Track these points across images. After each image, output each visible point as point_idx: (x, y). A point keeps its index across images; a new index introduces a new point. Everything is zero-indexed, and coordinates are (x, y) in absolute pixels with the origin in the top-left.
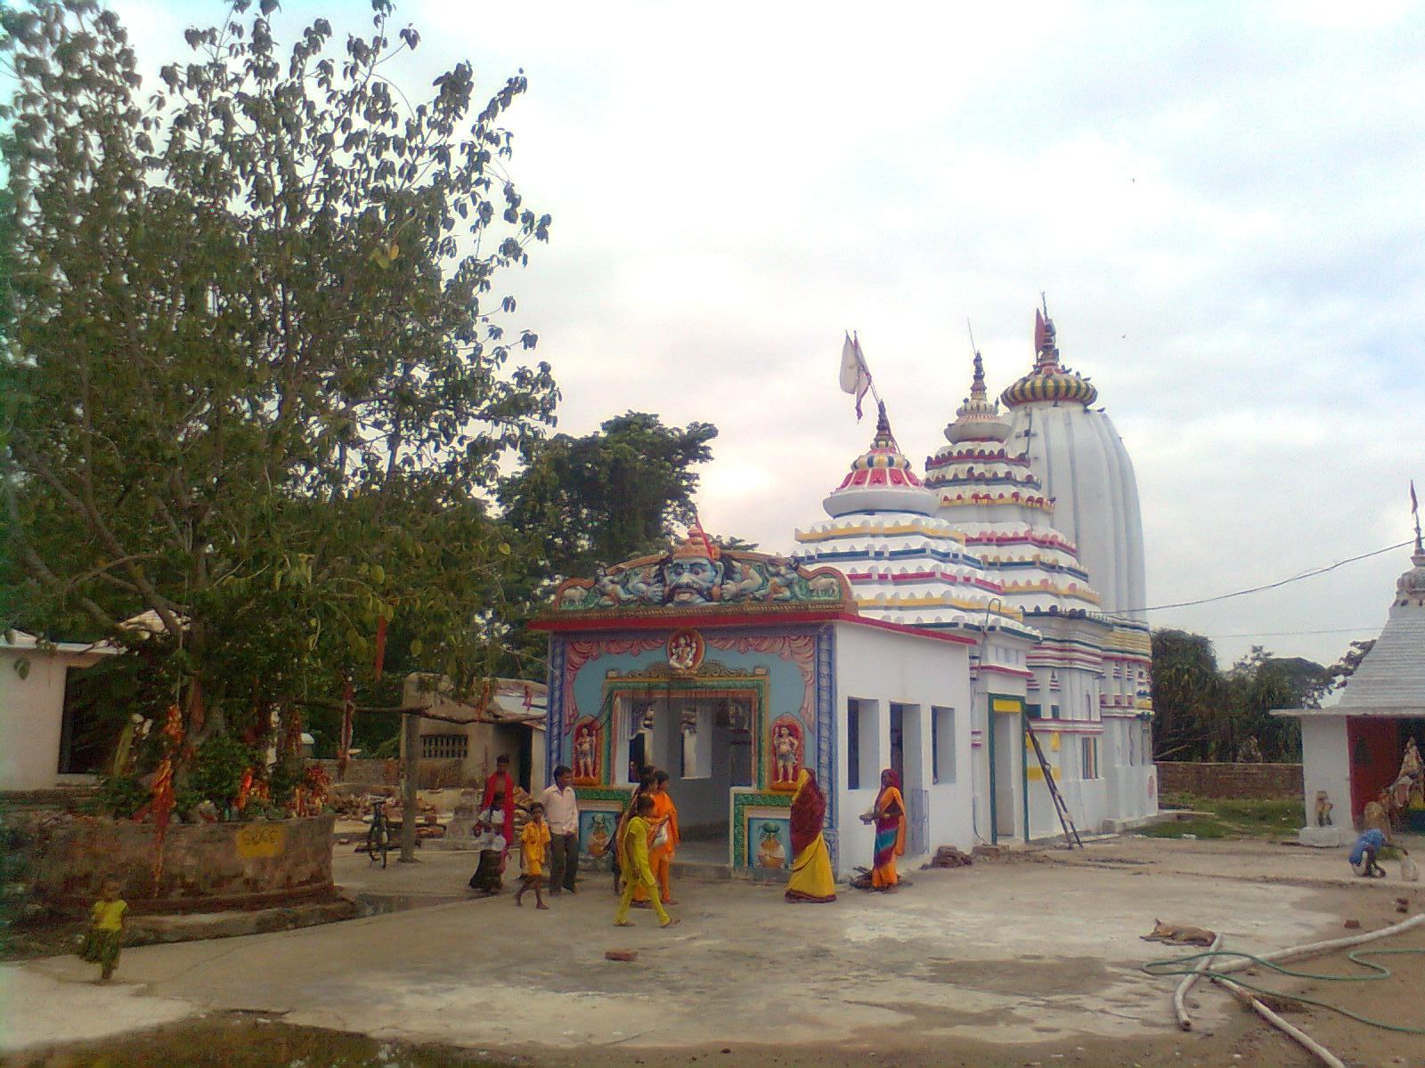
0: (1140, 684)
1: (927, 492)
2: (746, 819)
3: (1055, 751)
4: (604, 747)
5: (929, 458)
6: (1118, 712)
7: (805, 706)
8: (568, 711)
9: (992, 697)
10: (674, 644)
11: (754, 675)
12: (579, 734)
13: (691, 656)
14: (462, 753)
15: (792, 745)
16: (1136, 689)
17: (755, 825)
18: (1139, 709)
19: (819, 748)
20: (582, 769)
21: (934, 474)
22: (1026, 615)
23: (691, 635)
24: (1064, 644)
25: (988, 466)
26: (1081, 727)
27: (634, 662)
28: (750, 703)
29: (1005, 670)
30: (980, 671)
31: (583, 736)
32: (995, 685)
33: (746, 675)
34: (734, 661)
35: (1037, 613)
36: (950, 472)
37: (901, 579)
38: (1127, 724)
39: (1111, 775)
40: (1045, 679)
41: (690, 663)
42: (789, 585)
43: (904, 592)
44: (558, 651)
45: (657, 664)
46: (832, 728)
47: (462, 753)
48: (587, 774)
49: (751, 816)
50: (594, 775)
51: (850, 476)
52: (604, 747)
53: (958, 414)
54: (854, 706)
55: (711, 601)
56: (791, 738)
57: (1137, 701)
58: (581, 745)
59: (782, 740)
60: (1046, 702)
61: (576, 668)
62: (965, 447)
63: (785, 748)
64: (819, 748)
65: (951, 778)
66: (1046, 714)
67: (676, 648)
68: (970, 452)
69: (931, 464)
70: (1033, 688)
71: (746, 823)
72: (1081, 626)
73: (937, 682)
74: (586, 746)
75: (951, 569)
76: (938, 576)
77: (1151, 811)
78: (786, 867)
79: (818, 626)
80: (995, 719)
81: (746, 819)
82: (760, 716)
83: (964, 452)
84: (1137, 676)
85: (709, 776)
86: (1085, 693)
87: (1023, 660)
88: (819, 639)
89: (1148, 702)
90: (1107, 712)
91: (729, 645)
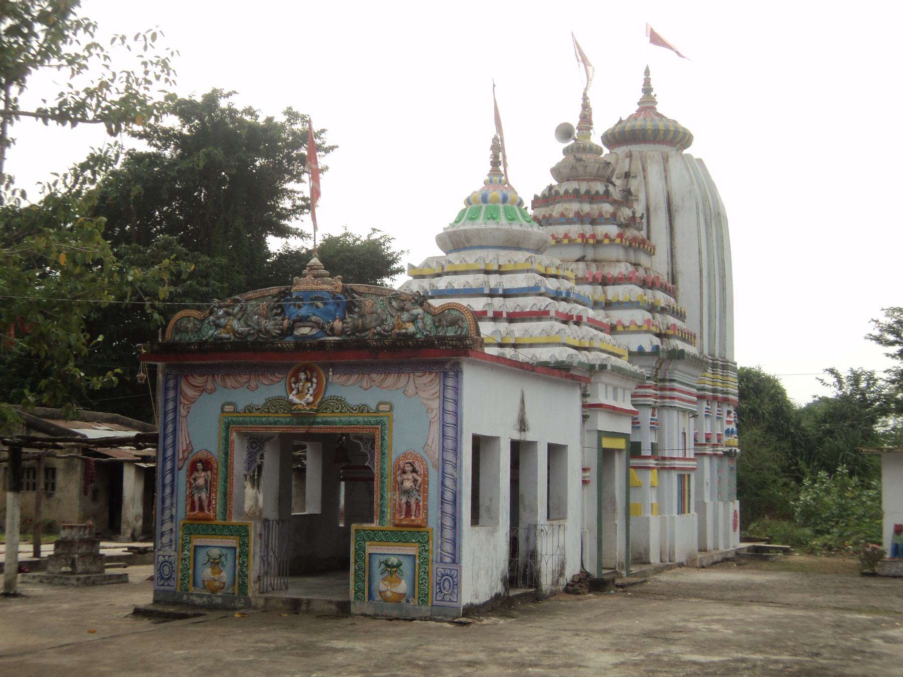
0: (729, 422)
1: (536, 229)
2: (367, 555)
3: (653, 487)
4: (220, 483)
5: (536, 196)
6: (709, 450)
7: (430, 442)
8: (182, 446)
9: (602, 434)
10: (293, 379)
11: (377, 410)
12: (193, 468)
13: (311, 392)
14: (50, 486)
15: (415, 481)
16: (722, 425)
17: (376, 564)
18: (726, 446)
19: (443, 484)
20: (197, 504)
21: (543, 211)
22: (631, 354)
23: (312, 370)
24: (662, 383)
25: (595, 206)
26: (677, 464)
27: (255, 394)
28: (374, 439)
29: (614, 408)
30: (589, 409)
31: (197, 471)
32: (604, 423)
33: (368, 412)
34: (356, 394)
35: (641, 352)
36: (557, 209)
37: (513, 318)
38: (716, 461)
39: (701, 508)
40: (646, 416)
41: (311, 399)
42: (414, 320)
43: (518, 329)
44: (171, 383)
45: (275, 399)
46: (457, 466)
47: (50, 486)
48: (202, 509)
49: (197, 544)
50: (209, 510)
51: (463, 212)
52: (220, 483)
53: (564, 153)
54: (479, 442)
55: (333, 335)
56: (414, 474)
57: (725, 439)
58: (195, 479)
59: (405, 476)
60: (647, 439)
61: (192, 401)
62: (572, 186)
63: (408, 484)
64: (443, 484)
65: (563, 516)
66: (646, 451)
67: (295, 383)
68: (576, 192)
69: (538, 202)
70: (636, 425)
71: (367, 559)
72: (680, 366)
73: (555, 418)
74: (201, 482)
75: (563, 307)
76: (552, 314)
77: (734, 542)
78: (408, 601)
79: (443, 363)
80: (606, 455)
81: (367, 555)
82: (383, 454)
83: (571, 191)
84: (725, 414)
85: (319, 512)
86: (681, 431)
87: (628, 398)
88: (445, 375)
89: (734, 440)
90: (701, 450)
91: (351, 382)
